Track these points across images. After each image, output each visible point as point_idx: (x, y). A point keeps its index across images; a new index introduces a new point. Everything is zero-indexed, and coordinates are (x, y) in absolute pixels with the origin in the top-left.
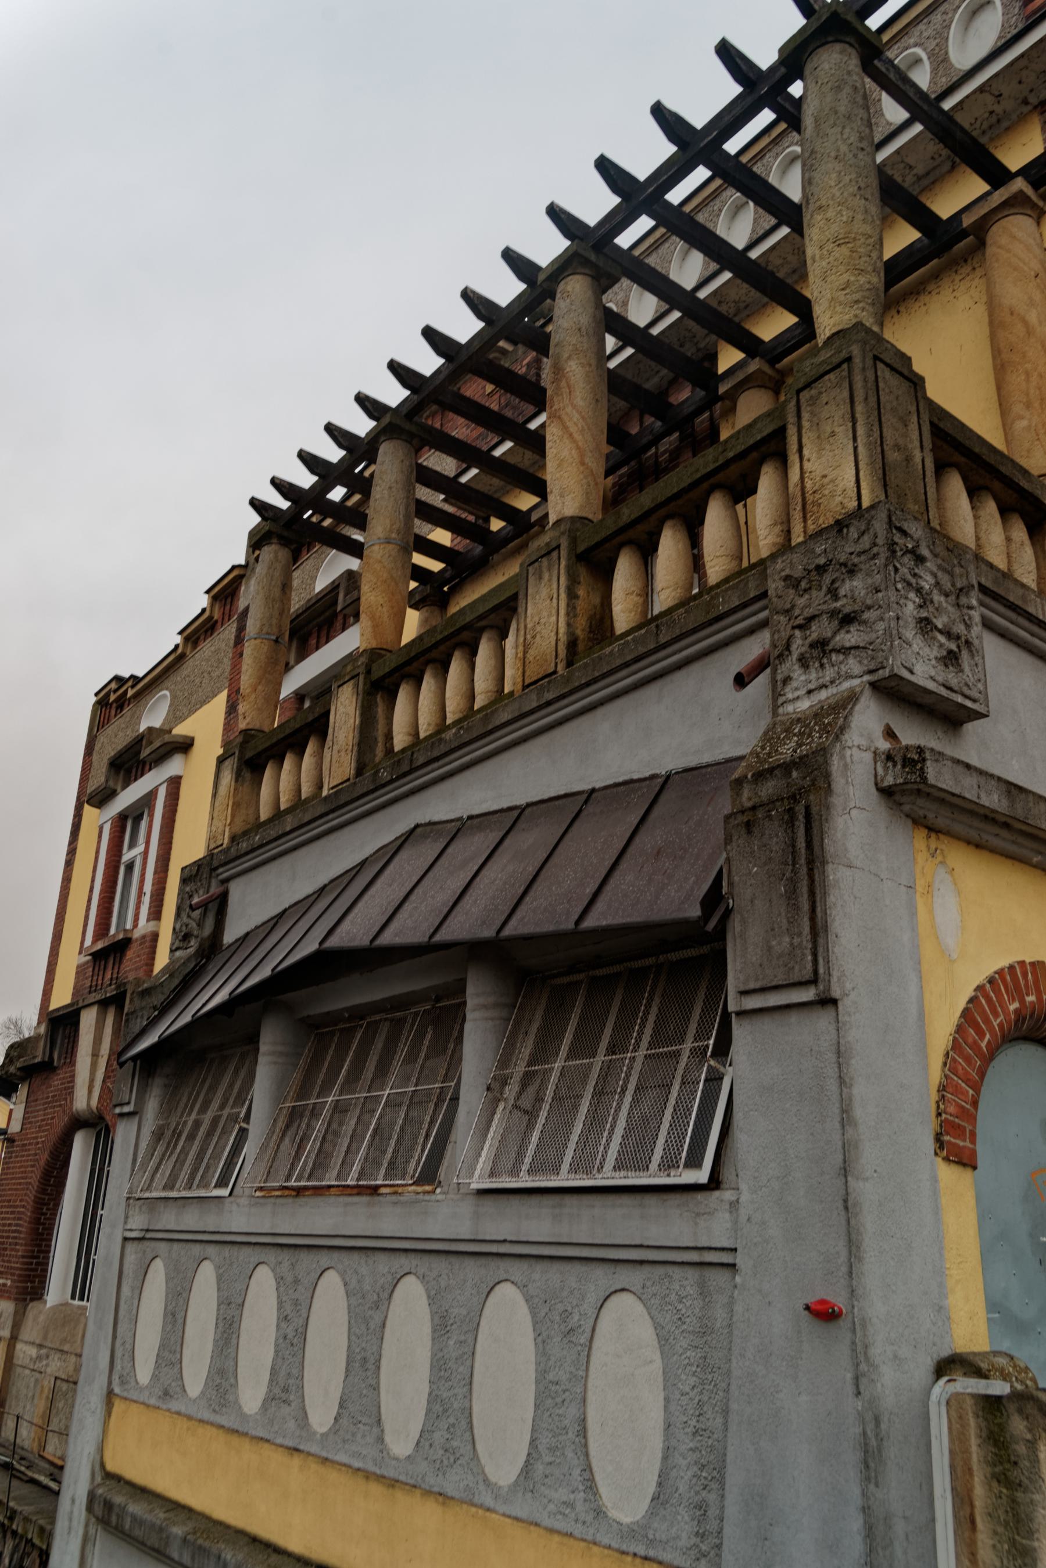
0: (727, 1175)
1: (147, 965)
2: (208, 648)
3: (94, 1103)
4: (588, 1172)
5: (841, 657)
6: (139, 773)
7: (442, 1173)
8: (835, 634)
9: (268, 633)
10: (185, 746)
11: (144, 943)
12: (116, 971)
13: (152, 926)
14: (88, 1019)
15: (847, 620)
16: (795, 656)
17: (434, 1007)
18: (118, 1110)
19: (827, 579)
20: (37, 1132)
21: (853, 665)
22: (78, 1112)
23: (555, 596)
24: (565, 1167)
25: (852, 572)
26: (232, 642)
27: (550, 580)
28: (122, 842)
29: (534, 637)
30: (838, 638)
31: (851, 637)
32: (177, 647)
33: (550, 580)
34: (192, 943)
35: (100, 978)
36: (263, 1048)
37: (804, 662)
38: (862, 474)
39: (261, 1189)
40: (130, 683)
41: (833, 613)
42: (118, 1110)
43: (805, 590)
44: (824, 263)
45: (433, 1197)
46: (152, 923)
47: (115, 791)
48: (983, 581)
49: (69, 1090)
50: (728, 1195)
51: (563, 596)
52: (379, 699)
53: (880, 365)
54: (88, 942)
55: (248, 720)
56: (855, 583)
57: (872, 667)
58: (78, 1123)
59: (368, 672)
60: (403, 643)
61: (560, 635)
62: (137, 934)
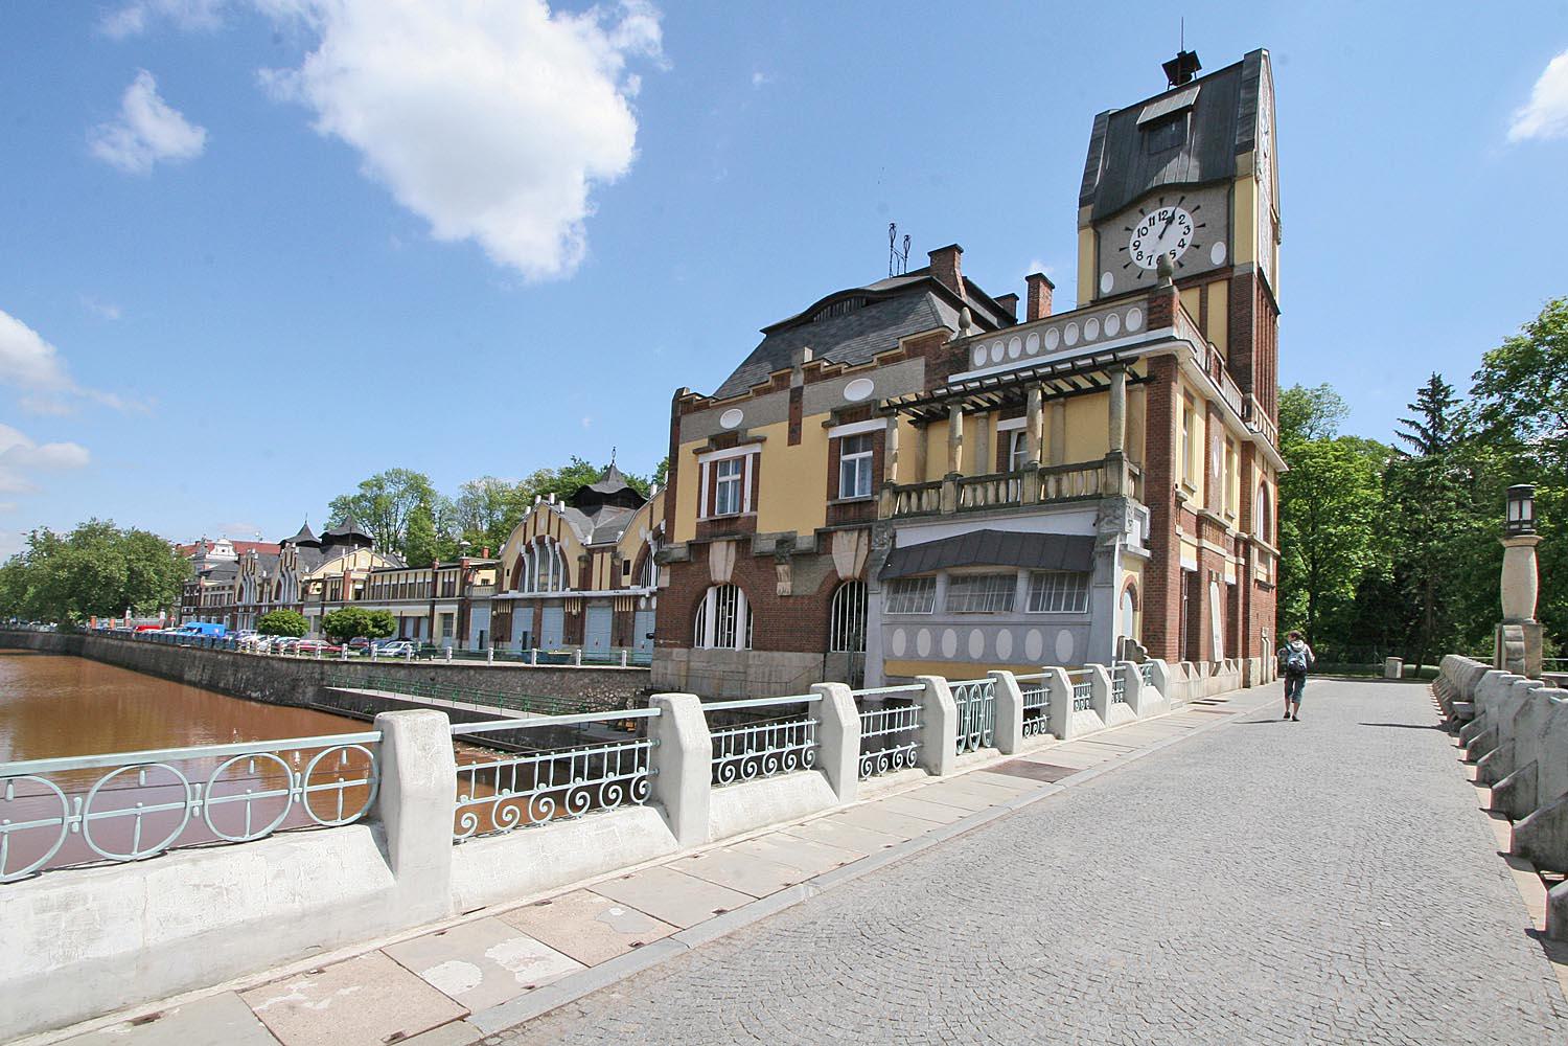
31: (1117, 521)
58: (713, 584)
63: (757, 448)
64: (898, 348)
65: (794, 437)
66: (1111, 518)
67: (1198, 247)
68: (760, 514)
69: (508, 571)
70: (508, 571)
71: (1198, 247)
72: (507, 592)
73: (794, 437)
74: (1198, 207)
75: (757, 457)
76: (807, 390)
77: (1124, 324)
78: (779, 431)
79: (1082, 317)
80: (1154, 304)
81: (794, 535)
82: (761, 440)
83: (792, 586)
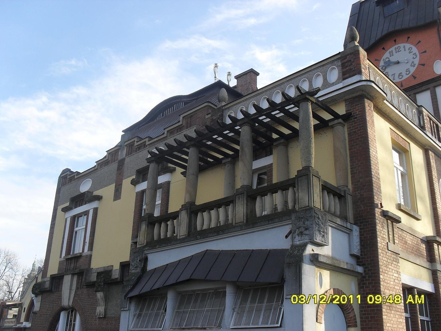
0: (283, 325)
1: (89, 264)
2: (106, 169)
3: (71, 304)
4: (255, 324)
5: (305, 236)
6: (81, 204)
7: (222, 325)
8: (304, 231)
9: (153, 188)
10: (99, 198)
11: (87, 257)
12: (75, 264)
13: (89, 253)
14: (67, 279)
15: (306, 229)
16: (297, 233)
17: (215, 291)
18: (122, 309)
19: (303, 220)
20: (46, 311)
21: (307, 237)
22: (64, 306)
23: (243, 204)
24: (251, 324)
25: (308, 220)
26: (116, 169)
27: (242, 200)
28: (74, 224)
29: (238, 212)
30: (305, 232)
31: (307, 232)
32: (95, 166)
33: (242, 200)
34: (138, 269)
35: (69, 266)
36: (168, 297)
37: (298, 235)
38: (309, 193)
39: (172, 328)
40: (76, 174)
41: (304, 227)
42: (122, 309)
43: (299, 221)
44: (303, 151)
45: (220, 330)
46: (89, 252)
47: (72, 208)
48: (329, 219)
49: (60, 298)
50: (283, 328)
51: (245, 205)
52: (192, 215)
53: (313, 176)
54: (64, 255)
55: (149, 211)
56: (308, 222)
57: (310, 239)
58: (64, 309)
59: (190, 208)
60: (124, 133)
61: (244, 214)
62: (84, 254)
63: (95, 204)
64: (179, 122)
65: (117, 195)
66: (302, 229)
67: (424, 65)
68: (94, 253)
69: (25, 308)
70: (25, 308)
71: (424, 65)
72: (22, 323)
73: (117, 195)
74: (420, 42)
75: (96, 210)
76: (127, 160)
77: (326, 79)
78: (108, 192)
79: (297, 79)
80: (346, 60)
81: (110, 268)
82: (99, 198)
83: (105, 310)
